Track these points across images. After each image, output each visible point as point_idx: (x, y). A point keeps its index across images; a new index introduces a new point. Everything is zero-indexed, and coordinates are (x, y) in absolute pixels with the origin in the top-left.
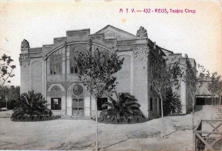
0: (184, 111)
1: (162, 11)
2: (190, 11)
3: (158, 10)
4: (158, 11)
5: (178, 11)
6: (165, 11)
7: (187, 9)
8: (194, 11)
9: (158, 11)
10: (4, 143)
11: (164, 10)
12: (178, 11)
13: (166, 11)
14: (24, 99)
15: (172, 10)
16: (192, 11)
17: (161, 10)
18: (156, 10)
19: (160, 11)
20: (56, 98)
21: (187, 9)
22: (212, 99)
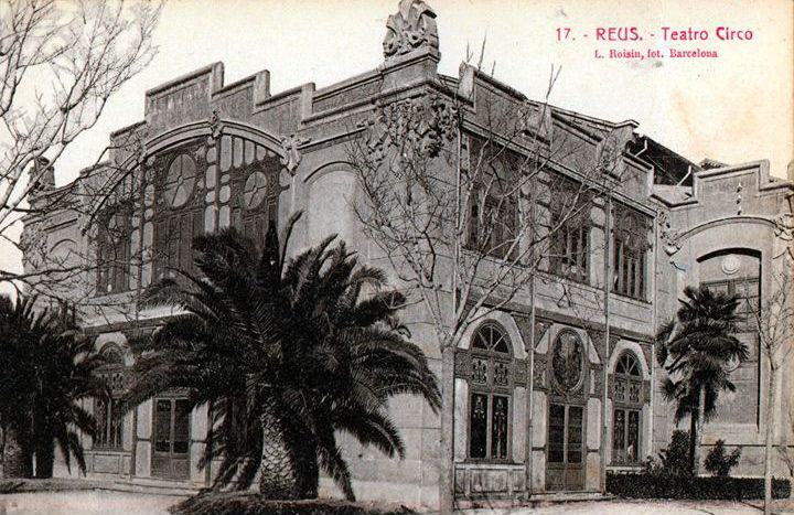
0: (594, 480)
1: (623, 35)
2: (735, 35)
3: (607, 31)
4: (606, 35)
5: (690, 32)
6: (630, 35)
7: (722, 28)
8: (704, 35)
9: (606, 35)
10: (122, 76)
11: (629, 32)
12: (690, 32)
13: (634, 37)
14: (152, 105)
15: (669, 34)
16: (742, 35)
17: (617, 31)
18: (601, 32)
19: (615, 36)
20: (219, 156)
21: (722, 28)
22: (480, 339)
